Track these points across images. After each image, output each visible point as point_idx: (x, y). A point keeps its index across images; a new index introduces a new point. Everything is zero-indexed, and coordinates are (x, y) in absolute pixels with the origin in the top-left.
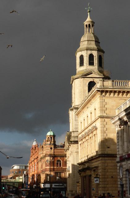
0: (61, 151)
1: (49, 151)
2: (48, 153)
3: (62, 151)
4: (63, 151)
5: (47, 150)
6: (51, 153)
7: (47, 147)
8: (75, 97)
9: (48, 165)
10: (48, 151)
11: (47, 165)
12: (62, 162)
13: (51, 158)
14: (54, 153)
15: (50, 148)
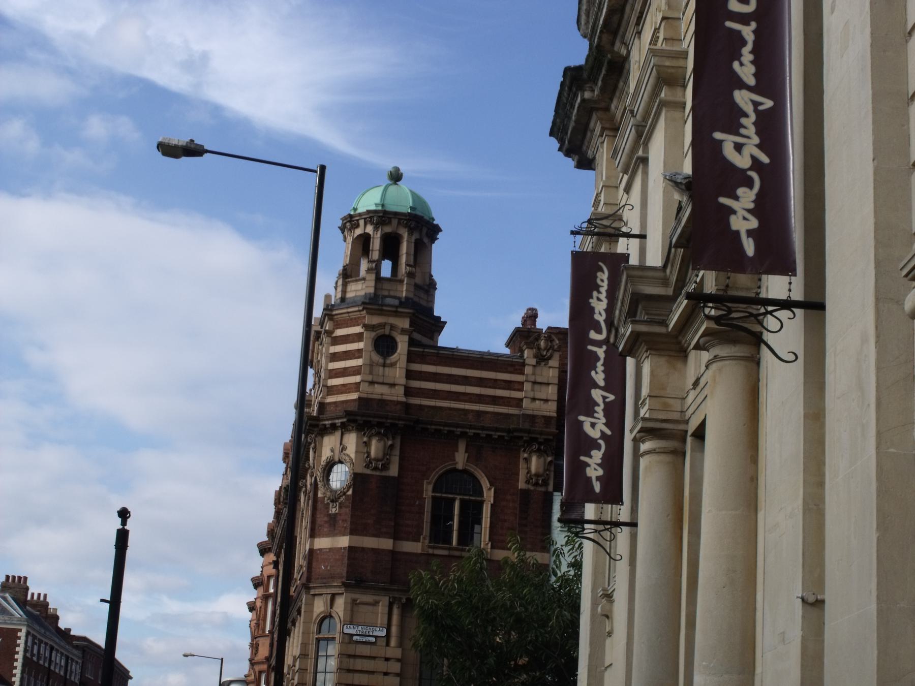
0: (481, 382)
1: (356, 371)
2: (345, 389)
3: (495, 384)
4: (508, 385)
5: (334, 357)
6: (380, 391)
7: (340, 332)
8: (766, 439)
9: (333, 519)
10: (344, 372)
11: (321, 519)
12: (489, 495)
13: (375, 448)
14: (408, 392)
15: (369, 336)
